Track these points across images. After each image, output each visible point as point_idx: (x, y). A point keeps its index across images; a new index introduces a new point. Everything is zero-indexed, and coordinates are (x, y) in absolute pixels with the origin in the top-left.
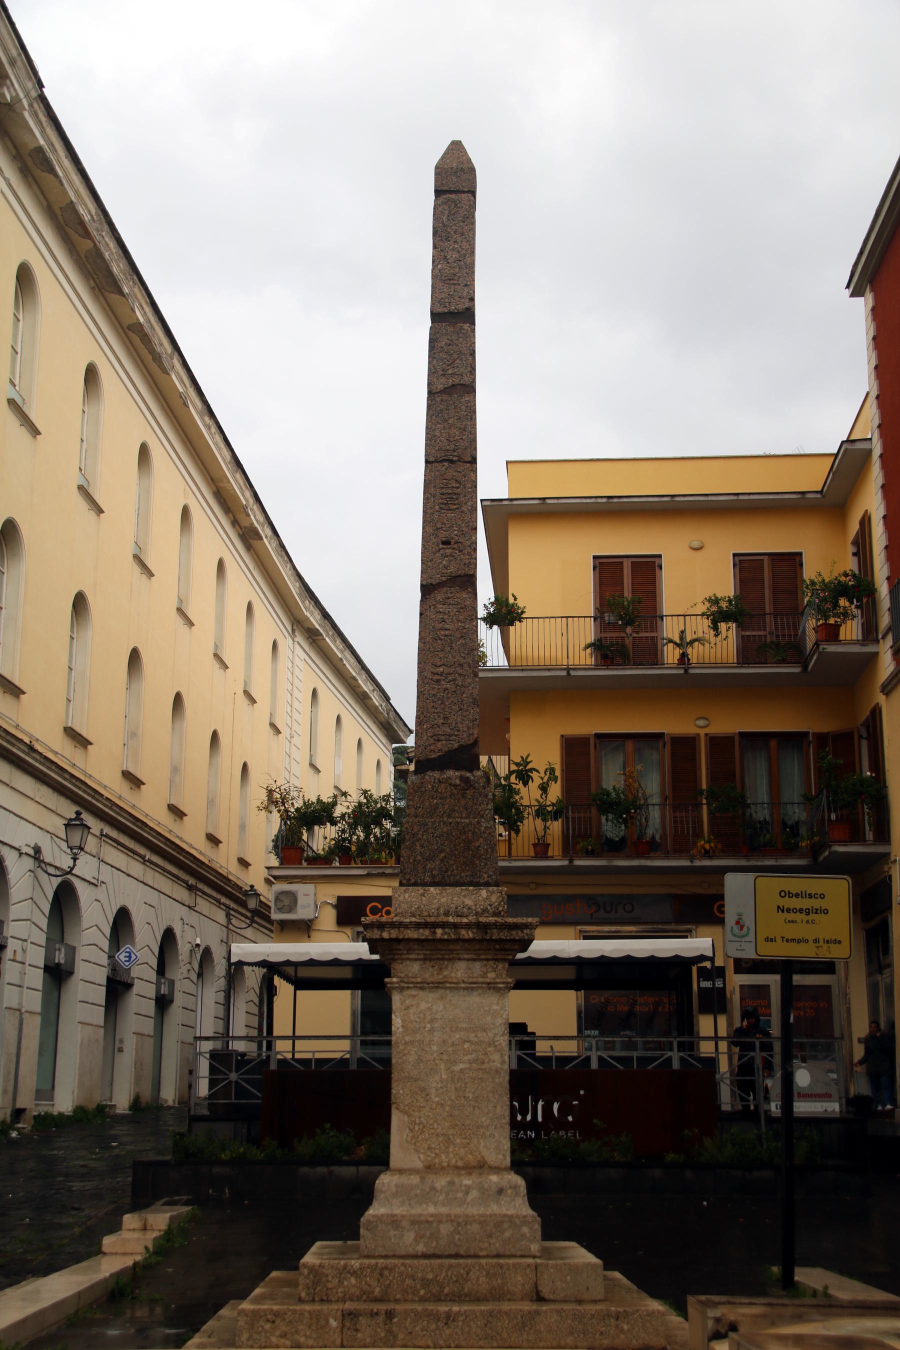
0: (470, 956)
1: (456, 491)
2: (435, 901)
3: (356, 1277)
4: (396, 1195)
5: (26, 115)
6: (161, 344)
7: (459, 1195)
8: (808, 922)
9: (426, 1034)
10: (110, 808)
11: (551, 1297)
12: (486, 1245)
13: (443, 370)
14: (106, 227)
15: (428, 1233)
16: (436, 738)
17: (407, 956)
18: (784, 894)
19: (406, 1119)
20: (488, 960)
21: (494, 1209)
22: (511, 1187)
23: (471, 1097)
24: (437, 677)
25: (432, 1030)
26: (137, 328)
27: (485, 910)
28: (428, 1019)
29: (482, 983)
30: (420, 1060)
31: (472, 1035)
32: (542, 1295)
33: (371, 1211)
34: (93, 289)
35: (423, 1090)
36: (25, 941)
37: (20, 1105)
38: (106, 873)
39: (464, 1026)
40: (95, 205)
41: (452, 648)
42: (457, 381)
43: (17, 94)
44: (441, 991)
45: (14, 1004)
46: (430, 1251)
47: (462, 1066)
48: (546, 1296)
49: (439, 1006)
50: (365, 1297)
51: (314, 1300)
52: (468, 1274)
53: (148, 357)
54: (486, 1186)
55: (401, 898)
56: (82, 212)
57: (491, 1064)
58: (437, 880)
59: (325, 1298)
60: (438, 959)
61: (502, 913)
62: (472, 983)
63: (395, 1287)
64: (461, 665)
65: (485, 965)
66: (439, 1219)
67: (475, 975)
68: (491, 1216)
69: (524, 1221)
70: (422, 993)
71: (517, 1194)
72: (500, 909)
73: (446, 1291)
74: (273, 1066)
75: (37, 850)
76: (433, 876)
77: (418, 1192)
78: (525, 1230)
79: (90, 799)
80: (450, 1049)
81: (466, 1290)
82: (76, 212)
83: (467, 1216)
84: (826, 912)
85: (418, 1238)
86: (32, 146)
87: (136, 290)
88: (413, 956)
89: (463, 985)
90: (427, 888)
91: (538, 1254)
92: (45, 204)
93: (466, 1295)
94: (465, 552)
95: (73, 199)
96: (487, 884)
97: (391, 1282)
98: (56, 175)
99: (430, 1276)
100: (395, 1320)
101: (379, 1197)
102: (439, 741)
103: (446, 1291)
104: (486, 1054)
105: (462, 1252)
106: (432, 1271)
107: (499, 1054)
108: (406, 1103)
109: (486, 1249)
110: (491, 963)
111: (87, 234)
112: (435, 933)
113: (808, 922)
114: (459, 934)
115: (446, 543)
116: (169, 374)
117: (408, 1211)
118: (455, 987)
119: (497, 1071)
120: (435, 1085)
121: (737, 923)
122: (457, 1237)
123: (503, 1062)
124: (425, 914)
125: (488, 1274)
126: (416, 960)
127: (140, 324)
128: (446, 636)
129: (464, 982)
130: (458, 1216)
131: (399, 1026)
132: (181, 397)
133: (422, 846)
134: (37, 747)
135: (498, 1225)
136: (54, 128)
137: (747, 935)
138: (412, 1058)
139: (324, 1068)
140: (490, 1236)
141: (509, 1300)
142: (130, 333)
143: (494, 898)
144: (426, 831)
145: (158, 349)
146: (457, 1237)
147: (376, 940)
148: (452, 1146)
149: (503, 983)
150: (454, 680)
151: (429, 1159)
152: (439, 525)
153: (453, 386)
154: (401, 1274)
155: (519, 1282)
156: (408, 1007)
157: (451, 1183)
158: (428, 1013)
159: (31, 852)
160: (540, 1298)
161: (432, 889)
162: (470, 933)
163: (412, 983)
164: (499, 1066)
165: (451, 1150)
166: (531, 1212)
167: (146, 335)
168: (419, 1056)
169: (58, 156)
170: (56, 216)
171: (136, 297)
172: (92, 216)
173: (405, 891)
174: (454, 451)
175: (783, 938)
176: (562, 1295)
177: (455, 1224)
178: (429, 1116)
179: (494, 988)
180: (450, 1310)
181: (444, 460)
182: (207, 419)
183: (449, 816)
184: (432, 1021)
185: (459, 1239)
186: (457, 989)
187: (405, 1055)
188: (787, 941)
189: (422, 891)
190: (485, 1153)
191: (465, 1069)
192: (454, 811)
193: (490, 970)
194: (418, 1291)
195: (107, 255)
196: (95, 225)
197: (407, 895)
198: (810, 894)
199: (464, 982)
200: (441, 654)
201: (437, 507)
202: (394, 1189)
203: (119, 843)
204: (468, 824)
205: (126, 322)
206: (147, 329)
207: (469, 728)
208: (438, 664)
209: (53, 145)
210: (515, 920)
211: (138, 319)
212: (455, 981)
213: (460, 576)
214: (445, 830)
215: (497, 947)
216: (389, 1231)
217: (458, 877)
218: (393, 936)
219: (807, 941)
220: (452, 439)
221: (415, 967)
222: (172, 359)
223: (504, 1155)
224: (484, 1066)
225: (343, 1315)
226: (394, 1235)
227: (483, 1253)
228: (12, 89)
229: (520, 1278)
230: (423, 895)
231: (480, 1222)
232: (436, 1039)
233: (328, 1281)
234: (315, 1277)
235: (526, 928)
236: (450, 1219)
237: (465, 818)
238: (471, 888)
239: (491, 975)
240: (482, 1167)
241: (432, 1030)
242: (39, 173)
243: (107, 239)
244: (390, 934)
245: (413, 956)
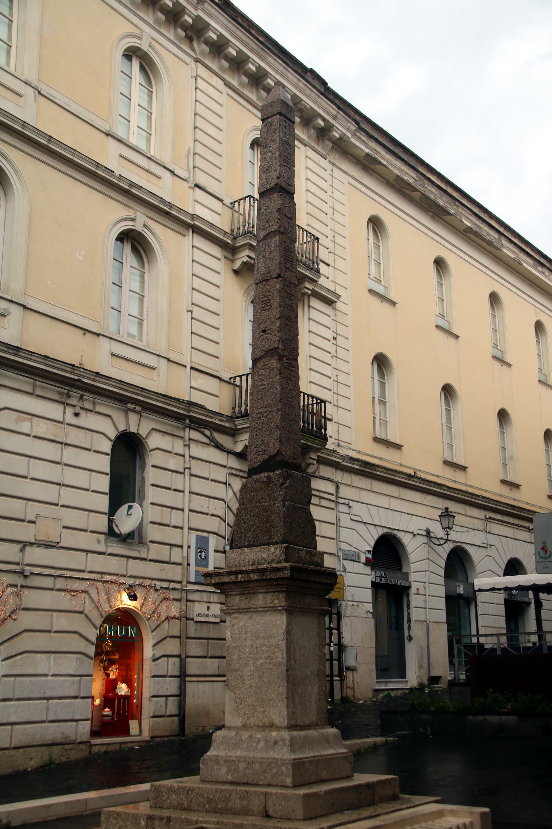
0: (263, 591)
1: (270, 297)
2: (247, 557)
3: (176, 794)
4: (222, 743)
5: (353, 140)
6: (489, 235)
7: (254, 744)
10: (489, 503)
11: (273, 815)
12: (263, 777)
14: (426, 182)
15: (233, 768)
16: (257, 454)
17: (230, 593)
20: (274, 592)
21: (272, 754)
24: (259, 416)
25: (246, 639)
26: (468, 230)
27: (273, 560)
28: (244, 632)
29: (270, 607)
30: (240, 657)
31: (267, 641)
32: (269, 813)
33: (208, 753)
34: (432, 216)
35: (241, 677)
36: (425, 583)
37: (434, 673)
38: (493, 540)
39: (262, 635)
40: (415, 172)
41: (266, 396)
42: (270, 230)
43: (342, 132)
44: (250, 614)
45: (422, 618)
47: (261, 661)
50: (180, 807)
51: (156, 807)
52: (230, 796)
53: (484, 244)
54: (268, 739)
55: (230, 557)
56: (406, 178)
58: (251, 543)
59: (161, 806)
60: (247, 593)
62: (263, 608)
63: (194, 802)
64: (271, 405)
65: (273, 596)
66: (239, 759)
67: (268, 602)
68: (267, 758)
70: (240, 616)
71: (284, 745)
73: (219, 806)
74: (545, 651)
75: (428, 532)
76: (249, 541)
77: (233, 741)
78: (284, 768)
79: (469, 499)
80: (255, 650)
81: (229, 807)
82: (403, 180)
83: (254, 758)
85: (229, 770)
86: (363, 155)
87: (460, 210)
88: (234, 593)
89: (260, 609)
90: (243, 549)
91: (291, 785)
92: (384, 181)
93: (229, 810)
94: (273, 334)
95: (398, 173)
97: (192, 798)
98: (383, 165)
99: (211, 796)
100: (171, 823)
101: (214, 744)
102: (259, 455)
103: (219, 806)
104: (274, 653)
105: (250, 782)
106: (212, 793)
107: (280, 653)
108: (233, 685)
109: (262, 780)
110: (276, 594)
111: (415, 190)
112: (237, 577)
114: (250, 577)
116: (501, 250)
117: (227, 753)
118: (257, 611)
119: (280, 664)
120: (247, 673)
121: (543, 549)
122: (248, 771)
123: (283, 658)
125: (240, 797)
126: (238, 595)
127: (469, 227)
128: (263, 389)
129: (260, 608)
130: (250, 758)
131: (229, 637)
132: (515, 260)
133: (245, 523)
134: (419, 474)
135: (269, 764)
136: (373, 141)
137: (550, 557)
138: (236, 657)
139: (483, 654)
140: (265, 772)
141: (251, 815)
142: (467, 234)
143: (278, 552)
145: (488, 238)
146: (248, 771)
149: (281, 606)
151: (244, 720)
153: (268, 233)
154: (197, 794)
155: (256, 804)
157: (251, 736)
158: (244, 628)
159: (425, 533)
160: (267, 816)
161: (246, 549)
163: (233, 609)
164: (281, 660)
165: (255, 715)
167: (475, 232)
169: (380, 154)
170: (393, 185)
171: (461, 213)
172: (414, 179)
173: (232, 553)
174: (268, 273)
176: (279, 814)
177: (247, 763)
180: (198, 820)
181: (263, 281)
182: (540, 268)
183: (260, 502)
185: (249, 773)
186: (258, 611)
187: (232, 655)
189: (240, 551)
190: (274, 717)
191: (263, 663)
192: (262, 498)
193: (276, 598)
194: (205, 805)
195: (432, 197)
196: (419, 183)
197: (233, 555)
200: (261, 401)
201: (260, 311)
202: (221, 739)
203: (503, 522)
205: (462, 229)
206: (475, 228)
207: (274, 444)
208: (259, 407)
209: (376, 150)
210: (277, 565)
211: (467, 225)
212: (255, 607)
213: (271, 350)
214: (257, 511)
215: (274, 583)
216: (214, 766)
217: (261, 541)
218: (217, 581)
221: (237, 599)
222: (500, 241)
224: (274, 661)
225: (147, 818)
226: (217, 768)
227: (261, 783)
228: (338, 131)
229: (257, 801)
230: (241, 554)
231: (260, 763)
232: (247, 644)
233: (163, 796)
235: (285, 570)
236: (245, 759)
237: (268, 502)
238: (266, 547)
239: (276, 602)
240: (272, 726)
241: (246, 639)
242: (373, 167)
243: (429, 188)
244: (215, 580)
245: (234, 593)
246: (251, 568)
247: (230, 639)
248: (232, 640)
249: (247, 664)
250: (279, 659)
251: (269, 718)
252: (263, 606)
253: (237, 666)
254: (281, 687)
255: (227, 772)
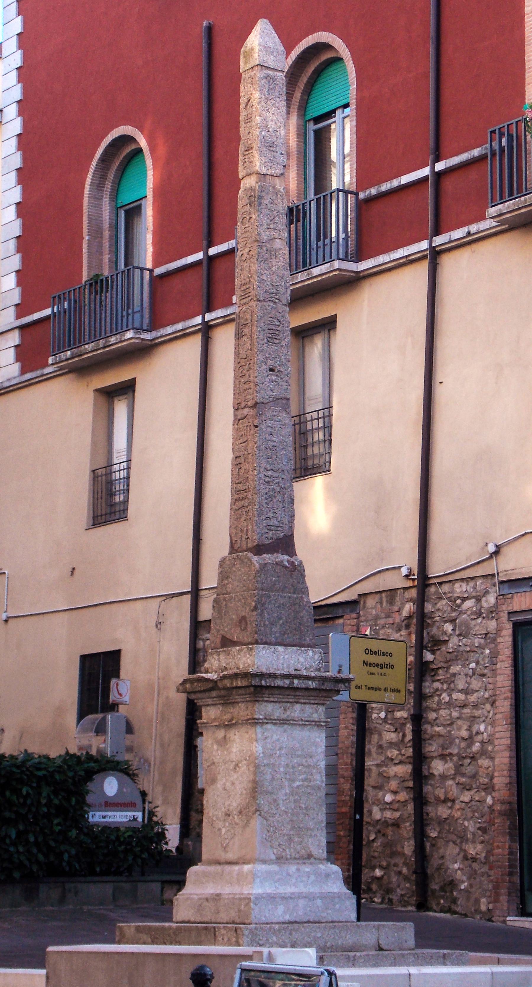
1: (279, 328)
8: (381, 674)
9: (276, 759)
13: (267, 224)
18: (369, 652)
19: (265, 822)
22: (333, 873)
23: (303, 806)
24: (267, 479)
30: (273, 779)
31: (304, 761)
35: (275, 801)
44: (286, 726)
46: (293, 919)
47: (298, 783)
48: (384, 948)
49: (284, 738)
57: (315, 782)
58: (278, 641)
61: (322, 669)
62: (305, 721)
69: (339, 896)
72: (320, 666)
76: (276, 638)
84: (392, 667)
89: (301, 723)
90: (276, 647)
96: (309, 646)
102: (270, 530)
108: (265, 810)
113: (381, 674)
115: (272, 370)
120: (282, 797)
123: (322, 781)
124: (275, 667)
128: (273, 446)
129: (302, 720)
138: (268, 777)
143: (316, 657)
144: (270, 601)
147: (258, 686)
148: (292, 843)
150: (278, 483)
152: (267, 355)
156: (266, 738)
160: (381, 949)
162: (314, 684)
164: (320, 784)
166: (348, 891)
168: (273, 776)
174: (276, 294)
175: (366, 686)
178: (278, 821)
179: (318, 726)
184: (280, 749)
188: (369, 688)
191: (300, 785)
198: (383, 653)
199: (302, 720)
204: (296, 598)
208: (269, 468)
217: (291, 639)
219: (380, 689)
220: (274, 284)
223: (323, 850)
232: (283, 763)
233: (260, 939)
234: (252, 936)
238: (303, 648)
244: (266, 682)
246: (313, 674)
247: (261, 755)
248: (264, 756)
249: (282, 787)
250: (318, 782)
251: (306, 849)
252: (306, 719)
253: (270, 788)
254: (320, 814)
255: (284, 912)
